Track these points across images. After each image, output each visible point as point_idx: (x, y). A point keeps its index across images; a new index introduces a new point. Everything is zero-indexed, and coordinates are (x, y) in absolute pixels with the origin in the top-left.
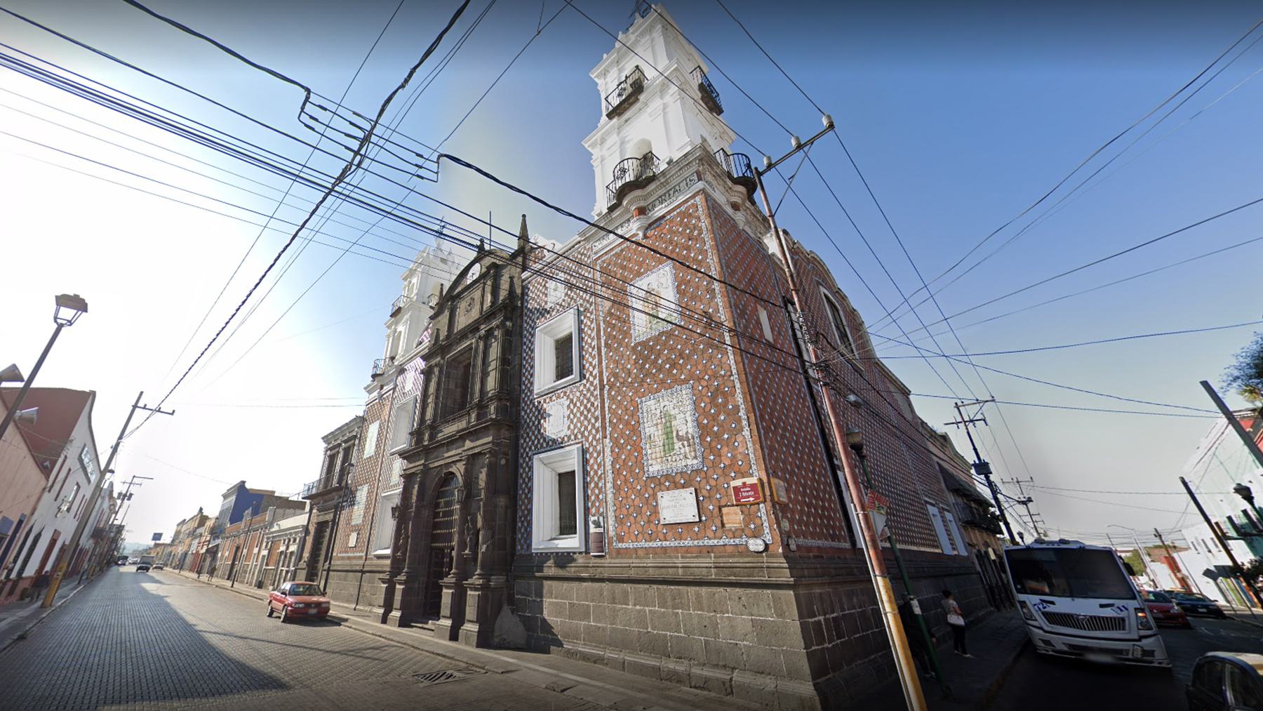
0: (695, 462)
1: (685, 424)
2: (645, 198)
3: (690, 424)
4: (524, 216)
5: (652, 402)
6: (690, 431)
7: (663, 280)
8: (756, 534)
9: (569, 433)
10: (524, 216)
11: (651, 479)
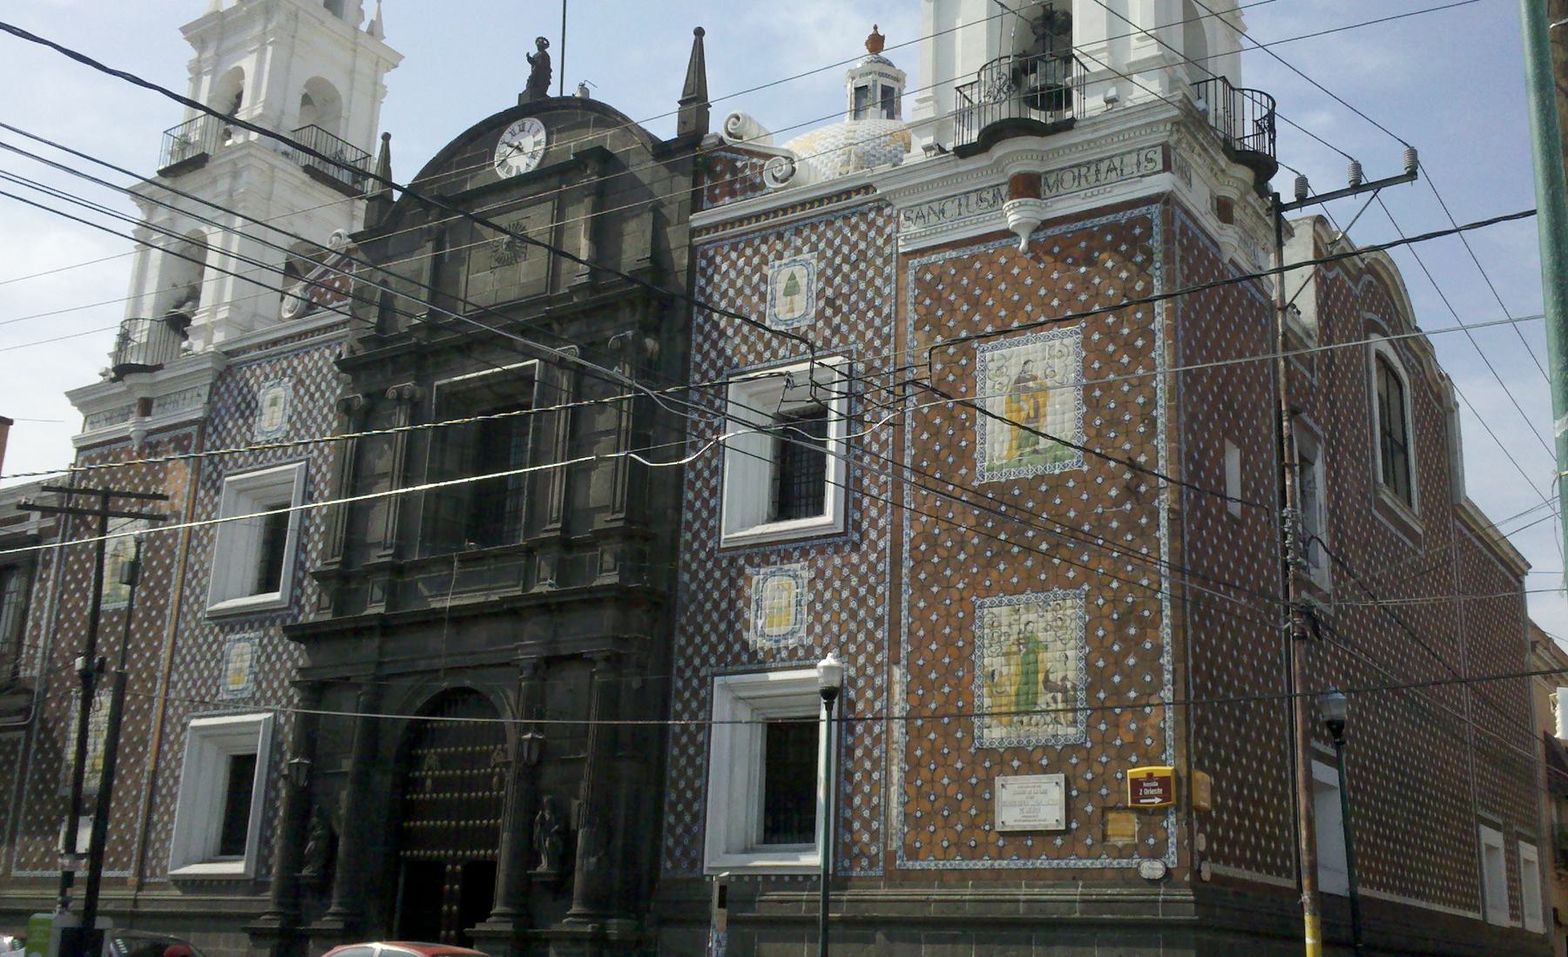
0: (1071, 731)
1: (1064, 660)
2: (1043, 156)
3: (1071, 664)
4: (699, 32)
5: (1005, 610)
6: (1071, 675)
7: (1057, 364)
8: (1156, 853)
9: (809, 641)
10: (699, 32)
11: (988, 752)
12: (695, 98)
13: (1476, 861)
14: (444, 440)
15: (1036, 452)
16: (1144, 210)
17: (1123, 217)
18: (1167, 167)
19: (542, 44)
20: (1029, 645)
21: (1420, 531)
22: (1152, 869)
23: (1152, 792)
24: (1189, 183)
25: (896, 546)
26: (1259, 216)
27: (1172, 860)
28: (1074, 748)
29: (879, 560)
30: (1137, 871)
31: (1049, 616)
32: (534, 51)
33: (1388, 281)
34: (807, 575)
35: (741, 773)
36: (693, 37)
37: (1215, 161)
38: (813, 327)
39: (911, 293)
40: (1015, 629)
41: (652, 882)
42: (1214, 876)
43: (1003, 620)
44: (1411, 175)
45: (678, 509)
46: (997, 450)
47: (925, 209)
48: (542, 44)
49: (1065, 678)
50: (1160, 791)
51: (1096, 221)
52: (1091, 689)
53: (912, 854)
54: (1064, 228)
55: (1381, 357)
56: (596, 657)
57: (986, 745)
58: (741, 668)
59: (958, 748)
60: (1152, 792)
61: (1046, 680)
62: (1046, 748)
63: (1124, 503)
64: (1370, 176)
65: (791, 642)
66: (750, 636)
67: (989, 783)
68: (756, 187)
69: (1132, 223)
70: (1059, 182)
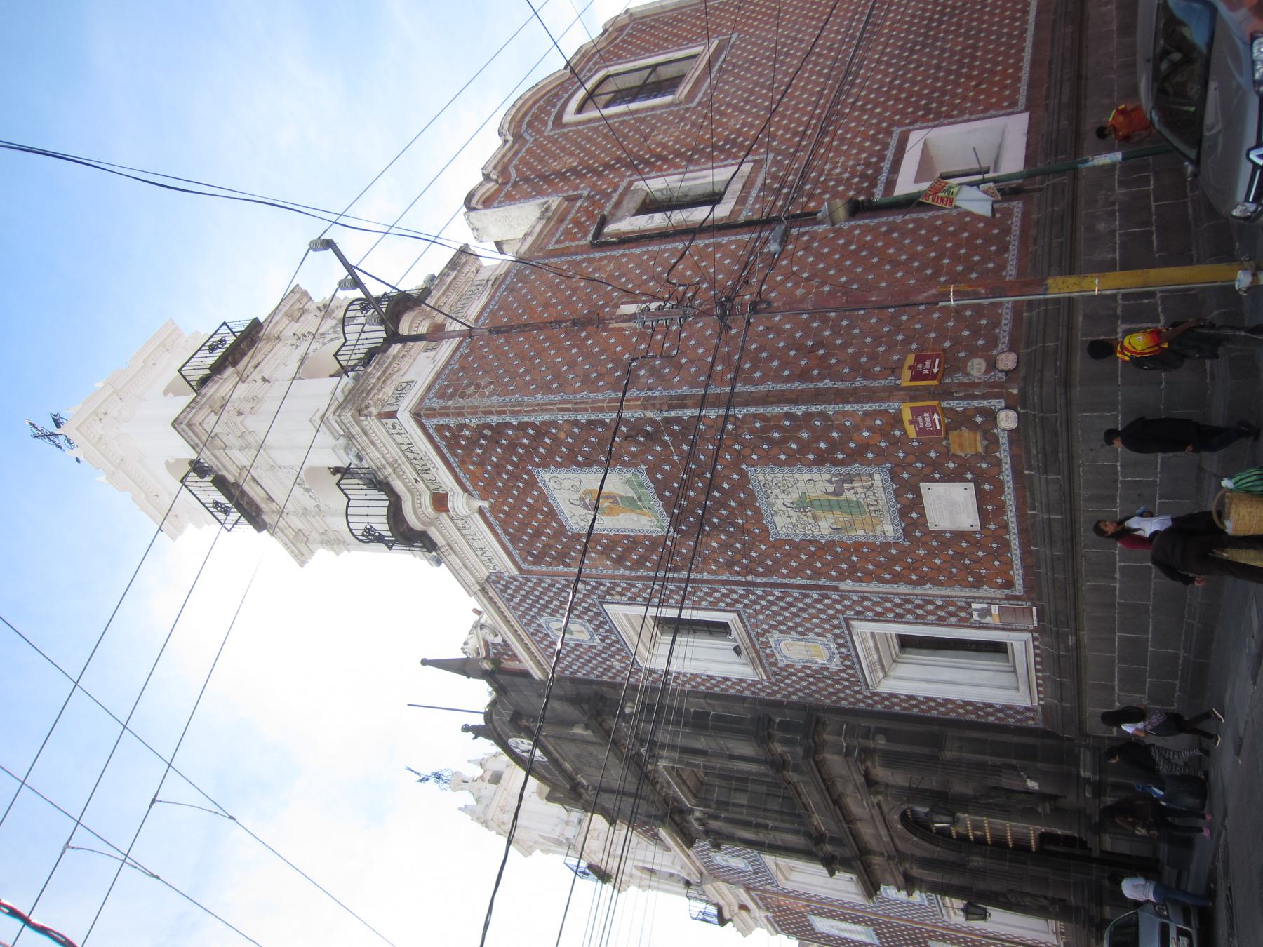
0: (877, 477)
3: (816, 477)
4: (425, 662)
5: (777, 519)
6: (828, 476)
7: (566, 484)
8: (991, 416)
10: (425, 662)
11: (907, 534)
12: (462, 667)
13: (967, 117)
14: (727, 804)
15: (640, 499)
16: (431, 431)
17: (442, 444)
18: (393, 415)
19: (466, 729)
20: (804, 504)
21: (716, 42)
22: (1008, 420)
23: (928, 420)
24: (410, 383)
25: (738, 584)
26: (448, 289)
27: (995, 403)
28: (894, 476)
29: (754, 594)
30: (1011, 432)
31: (776, 491)
32: (471, 735)
33: (530, 103)
34: (776, 634)
35: (947, 674)
36: (428, 667)
37: (395, 357)
38: (590, 622)
39: (543, 568)
40: (792, 513)
41: (1052, 735)
42: (1012, 348)
43: (783, 524)
44: (329, 244)
45: (744, 699)
46: (647, 521)
47: (483, 558)
48: (466, 729)
49: (829, 481)
50: (927, 415)
51: (451, 460)
52: (836, 463)
53: (1009, 584)
54: (464, 480)
55: (580, 110)
56: (862, 768)
57: (901, 534)
58: (859, 673)
59: (904, 552)
60: (928, 420)
61: (835, 493)
62: (898, 495)
63: (665, 442)
64: (343, 273)
65: (833, 646)
66: (833, 668)
67: (938, 535)
68: (506, 644)
69: (444, 438)
70: (432, 481)
